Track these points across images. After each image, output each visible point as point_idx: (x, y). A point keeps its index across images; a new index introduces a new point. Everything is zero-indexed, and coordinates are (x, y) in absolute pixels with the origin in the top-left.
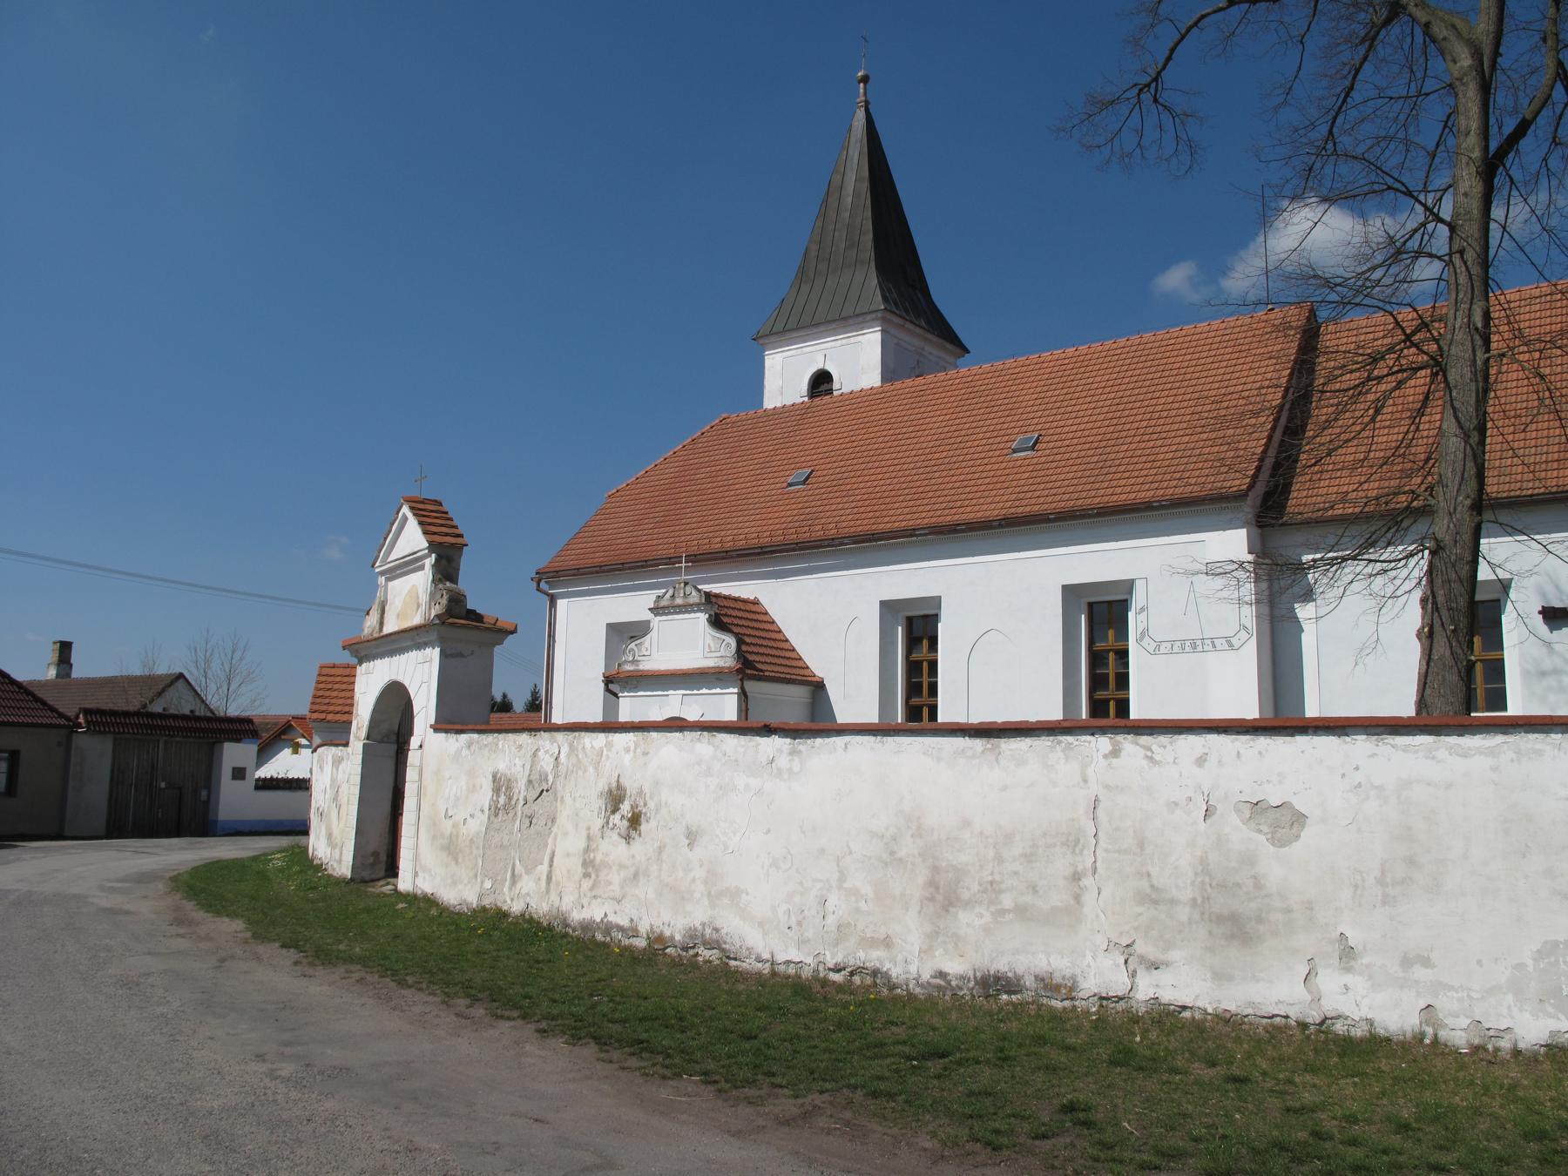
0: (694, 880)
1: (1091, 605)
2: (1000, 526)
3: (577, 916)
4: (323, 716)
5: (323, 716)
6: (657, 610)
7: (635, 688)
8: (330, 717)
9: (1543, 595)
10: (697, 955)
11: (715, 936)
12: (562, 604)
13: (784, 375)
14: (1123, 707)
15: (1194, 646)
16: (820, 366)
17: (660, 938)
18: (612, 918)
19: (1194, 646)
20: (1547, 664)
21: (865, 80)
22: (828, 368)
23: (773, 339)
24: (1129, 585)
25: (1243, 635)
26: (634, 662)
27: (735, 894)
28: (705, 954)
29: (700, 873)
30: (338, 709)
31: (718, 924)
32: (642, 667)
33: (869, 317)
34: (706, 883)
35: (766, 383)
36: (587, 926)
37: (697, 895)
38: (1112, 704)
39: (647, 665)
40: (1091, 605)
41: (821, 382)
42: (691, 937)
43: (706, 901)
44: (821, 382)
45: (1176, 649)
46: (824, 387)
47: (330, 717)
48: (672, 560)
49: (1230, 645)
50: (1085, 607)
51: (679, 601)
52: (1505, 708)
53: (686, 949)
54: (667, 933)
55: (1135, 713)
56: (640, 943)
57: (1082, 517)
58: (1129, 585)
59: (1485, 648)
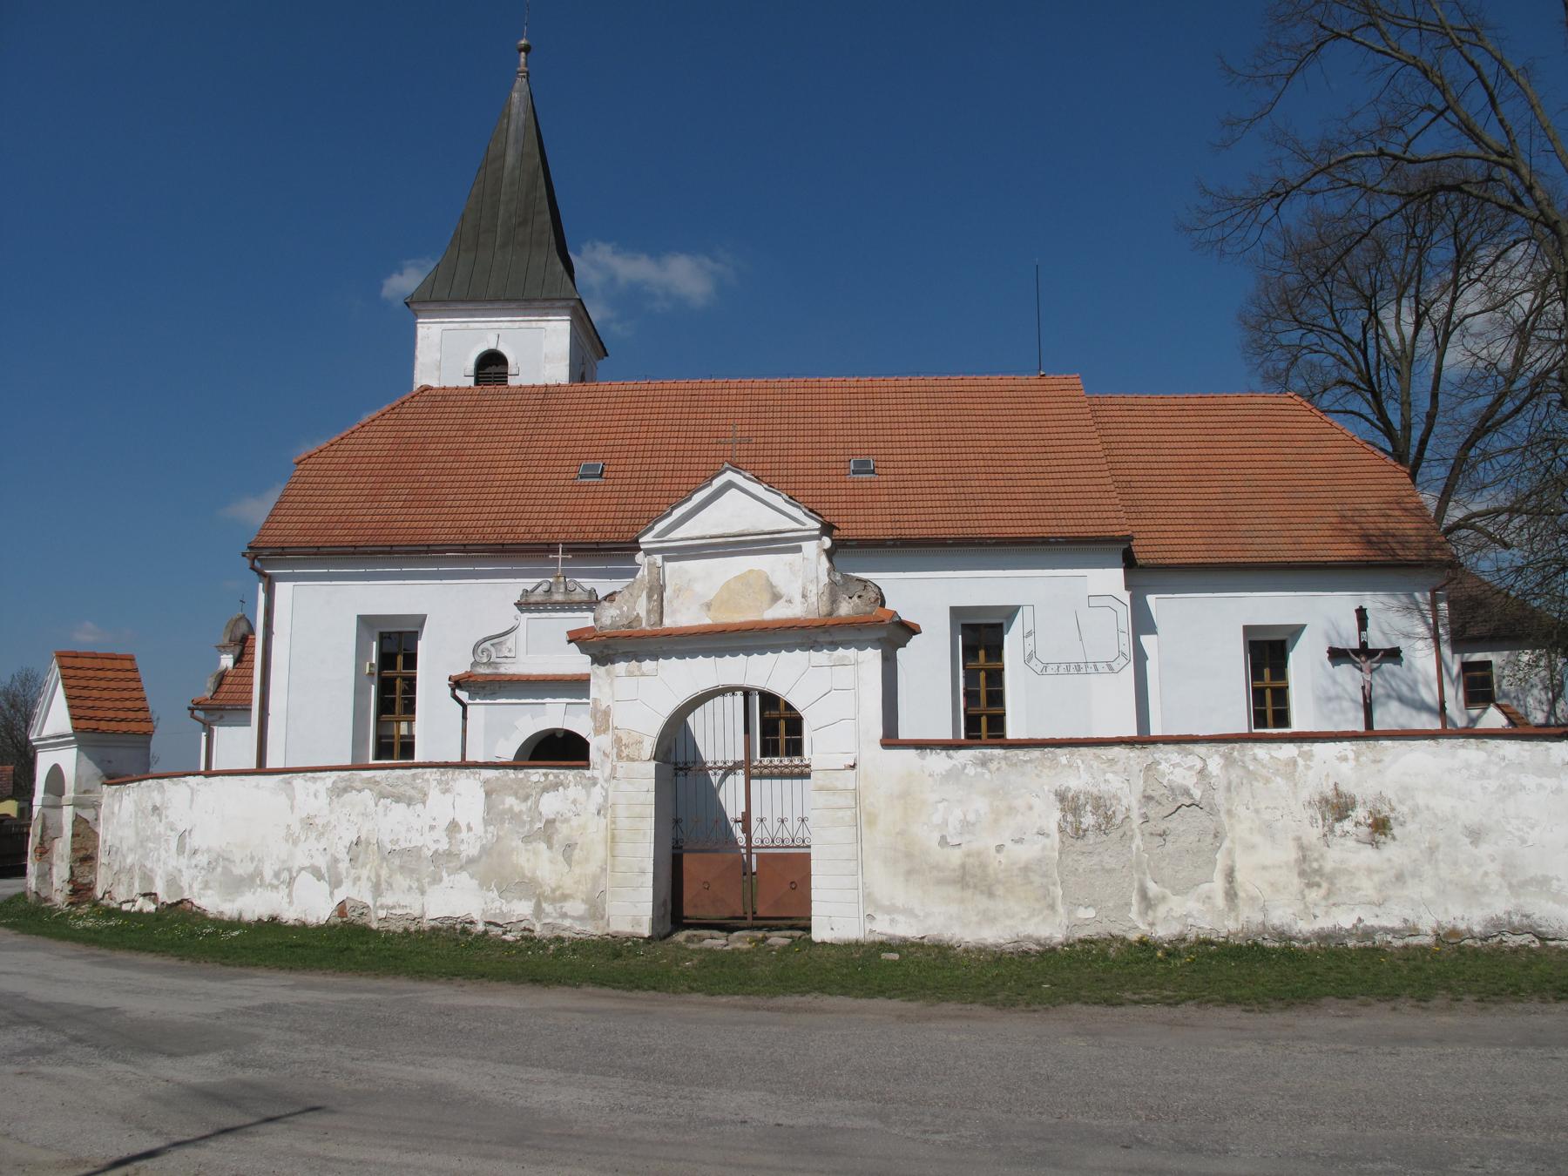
0: (1486, 874)
1: (381, 634)
2: (894, 546)
3: (1305, 927)
4: (93, 724)
5: (93, 724)
6: (524, 605)
7: (493, 694)
8: (103, 725)
9: (1328, 637)
10: (1501, 941)
11: (1525, 922)
12: (283, 590)
13: (444, 350)
14: (997, 723)
15: (1078, 669)
16: (492, 346)
17: (1454, 932)
18: (1370, 922)
19: (1078, 669)
20: (1332, 692)
21: (527, 49)
22: (504, 349)
23: (432, 306)
24: (421, 620)
25: (1122, 661)
26: (489, 664)
27: (1543, 882)
28: (1513, 941)
29: (1492, 867)
30: (111, 714)
31: (1528, 910)
32: (502, 670)
33: (558, 304)
34: (1503, 875)
35: (418, 353)
36: (1323, 936)
37: (1494, 887)
38: (984, 720)
39: (508, 669)
40: (381, 634)
41: (491, 365)
42: (1495, 926)
43: (1506, 892)
44: (491, 365)
45: (1049, 671)
46: (492, 369)
47: (124, 727)
48: (550, 548)
49: (1111, 668)
50: (377, 636)
51: (558, 597)
52: (412, 757)
53: (1486, 939)
54: (1462, 926)
55: (1011, 733)
56: (1427, 940)
57: (981, 545)
58: (421, 620)
59: (1272, 678)
